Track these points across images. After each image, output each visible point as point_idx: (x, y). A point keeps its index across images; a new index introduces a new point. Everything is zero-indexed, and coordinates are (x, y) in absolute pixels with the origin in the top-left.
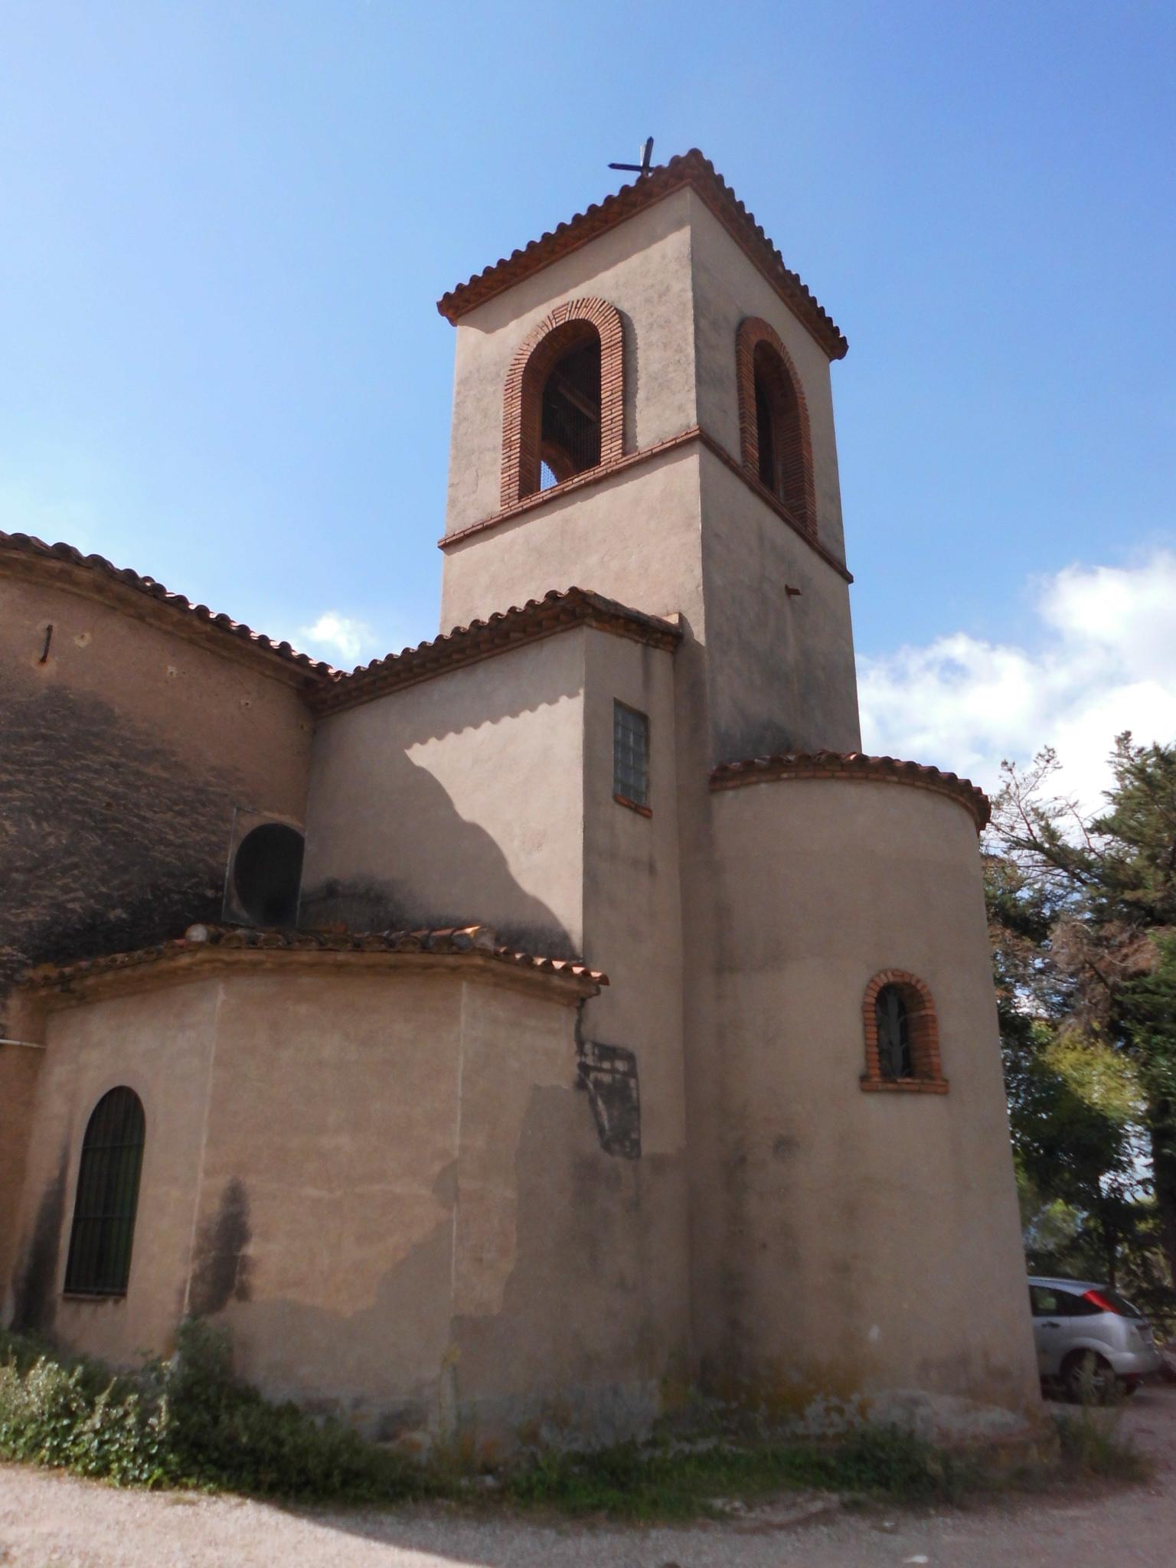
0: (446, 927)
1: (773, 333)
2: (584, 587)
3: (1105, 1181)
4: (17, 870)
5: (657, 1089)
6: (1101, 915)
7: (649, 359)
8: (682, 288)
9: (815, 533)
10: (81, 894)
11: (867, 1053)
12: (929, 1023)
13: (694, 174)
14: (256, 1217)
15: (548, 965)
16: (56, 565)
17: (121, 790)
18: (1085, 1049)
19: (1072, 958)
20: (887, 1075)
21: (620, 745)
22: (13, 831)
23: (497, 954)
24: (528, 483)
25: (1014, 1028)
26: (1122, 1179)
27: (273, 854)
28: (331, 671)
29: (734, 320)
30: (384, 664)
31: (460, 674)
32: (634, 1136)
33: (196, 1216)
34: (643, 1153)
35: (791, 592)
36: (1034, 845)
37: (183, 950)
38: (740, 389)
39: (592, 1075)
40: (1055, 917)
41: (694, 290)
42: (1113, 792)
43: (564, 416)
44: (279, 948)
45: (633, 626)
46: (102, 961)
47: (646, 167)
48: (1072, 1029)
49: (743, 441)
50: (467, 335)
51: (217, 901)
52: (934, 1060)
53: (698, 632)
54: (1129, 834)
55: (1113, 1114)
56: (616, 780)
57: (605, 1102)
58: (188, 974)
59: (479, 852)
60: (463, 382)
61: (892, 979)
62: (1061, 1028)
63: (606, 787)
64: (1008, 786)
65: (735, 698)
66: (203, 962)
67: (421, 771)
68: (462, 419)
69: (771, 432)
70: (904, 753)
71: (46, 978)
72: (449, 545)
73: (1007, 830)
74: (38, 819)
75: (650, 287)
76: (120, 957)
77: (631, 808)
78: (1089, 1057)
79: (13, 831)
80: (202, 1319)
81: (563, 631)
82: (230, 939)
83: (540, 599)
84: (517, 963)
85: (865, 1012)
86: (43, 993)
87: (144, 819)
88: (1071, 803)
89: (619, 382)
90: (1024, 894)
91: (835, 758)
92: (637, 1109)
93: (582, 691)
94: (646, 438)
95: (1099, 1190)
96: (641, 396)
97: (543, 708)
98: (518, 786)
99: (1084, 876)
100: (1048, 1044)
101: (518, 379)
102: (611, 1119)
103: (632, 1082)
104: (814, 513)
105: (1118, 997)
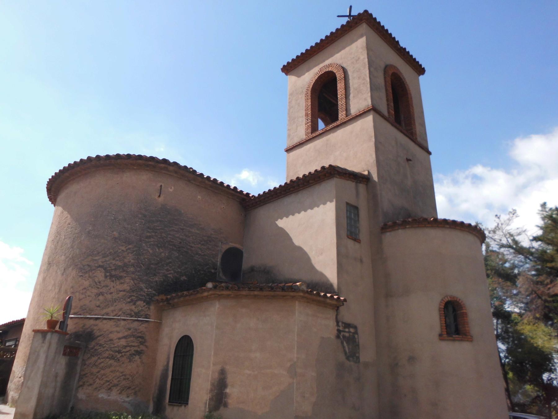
0: (291, 282)
1: (398, 69)
2: (333, 164)
3: (545, 376)
4: (152, 264)
5: (365, 338)
6: (539, 273)
7: (353, 83)
8: (364, 57)
9: (416, 139)
10: (172, 272)
11: (441, 326)
12: (465, 315)
13: (366, 18)
14: (230, 379)
15: (325, 295)
16: (162, 165)
17: (184, 237)
18: (534, 324)
19: (527, 290)
20: (449, 334)
21: (349, 218)
22: (151, 251)
23: (307, 292)
24: (314, 127)
25: (502, 315)
26: (553, 376)
27: (233, 257)
28: (251, 195)
29: (383, 66)
30: (268, 193)
31: (293, 195)
32: (357, 355)
33: (210, 379)
34: (361, 361)
35: (408, 160)
36: (510, 247)
37: (205, 291)
38: (386, 90)
39: (342, 333)
40: (519, 274)
41: (368, 58)
42: (540, 225)
43: (326, 102)
44: (235, 290)
45: (352, 176)
46: (179, 294)
47: (350, 16)
48: (529, 317)
49: (388, 109)
50: (292, 79)
51: (215, 273)
52: (467, 329)
53: (375, 177)
54: (547, 241)
55: (547, 350)
56: (348, 230)
57: (347, 343)
58: (207, 298)
59: (302, 256)
60: (291, 94)
61: (450, 299)
62: (524, 317)
63: (344, 233)
64: (498, 224)
65: (389, 199)
66: (212, 294)
67: (282, 229)
68: (291, 107)
69: (399, 105)
70: (451, 218)
71: (162, 299)
72: (288, 150)
73: (498, 241)
74: (159, 248)
75: (353, 59)
76: (185, 293)
77: (352, 239)
78: (535, 328)
79: (151, 251)
80: (212, 413)
81: (328, 179)
82: (220, 287)
83: (319, 169)
84: (314, 295)
85: (440, 311)
86: (161, 304)
87: (192, 247)
88: (524, 229)
89: (344, 92)
90: (507, 265)
91: (425, 220)
92: (358, 345)
93: (334, 200)
94: (354, 111)
95: (543, 380)
96: (351, 96)
97: (322, 206)
98: (314, 234)
99: (531, 257)
100: (519, 322)
101: (309, 92)
102: (349, 349)
103: (356, 336)
104: (416, 131)
105: (547, 304)
